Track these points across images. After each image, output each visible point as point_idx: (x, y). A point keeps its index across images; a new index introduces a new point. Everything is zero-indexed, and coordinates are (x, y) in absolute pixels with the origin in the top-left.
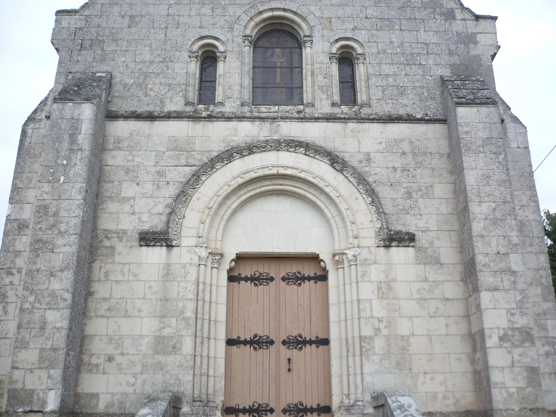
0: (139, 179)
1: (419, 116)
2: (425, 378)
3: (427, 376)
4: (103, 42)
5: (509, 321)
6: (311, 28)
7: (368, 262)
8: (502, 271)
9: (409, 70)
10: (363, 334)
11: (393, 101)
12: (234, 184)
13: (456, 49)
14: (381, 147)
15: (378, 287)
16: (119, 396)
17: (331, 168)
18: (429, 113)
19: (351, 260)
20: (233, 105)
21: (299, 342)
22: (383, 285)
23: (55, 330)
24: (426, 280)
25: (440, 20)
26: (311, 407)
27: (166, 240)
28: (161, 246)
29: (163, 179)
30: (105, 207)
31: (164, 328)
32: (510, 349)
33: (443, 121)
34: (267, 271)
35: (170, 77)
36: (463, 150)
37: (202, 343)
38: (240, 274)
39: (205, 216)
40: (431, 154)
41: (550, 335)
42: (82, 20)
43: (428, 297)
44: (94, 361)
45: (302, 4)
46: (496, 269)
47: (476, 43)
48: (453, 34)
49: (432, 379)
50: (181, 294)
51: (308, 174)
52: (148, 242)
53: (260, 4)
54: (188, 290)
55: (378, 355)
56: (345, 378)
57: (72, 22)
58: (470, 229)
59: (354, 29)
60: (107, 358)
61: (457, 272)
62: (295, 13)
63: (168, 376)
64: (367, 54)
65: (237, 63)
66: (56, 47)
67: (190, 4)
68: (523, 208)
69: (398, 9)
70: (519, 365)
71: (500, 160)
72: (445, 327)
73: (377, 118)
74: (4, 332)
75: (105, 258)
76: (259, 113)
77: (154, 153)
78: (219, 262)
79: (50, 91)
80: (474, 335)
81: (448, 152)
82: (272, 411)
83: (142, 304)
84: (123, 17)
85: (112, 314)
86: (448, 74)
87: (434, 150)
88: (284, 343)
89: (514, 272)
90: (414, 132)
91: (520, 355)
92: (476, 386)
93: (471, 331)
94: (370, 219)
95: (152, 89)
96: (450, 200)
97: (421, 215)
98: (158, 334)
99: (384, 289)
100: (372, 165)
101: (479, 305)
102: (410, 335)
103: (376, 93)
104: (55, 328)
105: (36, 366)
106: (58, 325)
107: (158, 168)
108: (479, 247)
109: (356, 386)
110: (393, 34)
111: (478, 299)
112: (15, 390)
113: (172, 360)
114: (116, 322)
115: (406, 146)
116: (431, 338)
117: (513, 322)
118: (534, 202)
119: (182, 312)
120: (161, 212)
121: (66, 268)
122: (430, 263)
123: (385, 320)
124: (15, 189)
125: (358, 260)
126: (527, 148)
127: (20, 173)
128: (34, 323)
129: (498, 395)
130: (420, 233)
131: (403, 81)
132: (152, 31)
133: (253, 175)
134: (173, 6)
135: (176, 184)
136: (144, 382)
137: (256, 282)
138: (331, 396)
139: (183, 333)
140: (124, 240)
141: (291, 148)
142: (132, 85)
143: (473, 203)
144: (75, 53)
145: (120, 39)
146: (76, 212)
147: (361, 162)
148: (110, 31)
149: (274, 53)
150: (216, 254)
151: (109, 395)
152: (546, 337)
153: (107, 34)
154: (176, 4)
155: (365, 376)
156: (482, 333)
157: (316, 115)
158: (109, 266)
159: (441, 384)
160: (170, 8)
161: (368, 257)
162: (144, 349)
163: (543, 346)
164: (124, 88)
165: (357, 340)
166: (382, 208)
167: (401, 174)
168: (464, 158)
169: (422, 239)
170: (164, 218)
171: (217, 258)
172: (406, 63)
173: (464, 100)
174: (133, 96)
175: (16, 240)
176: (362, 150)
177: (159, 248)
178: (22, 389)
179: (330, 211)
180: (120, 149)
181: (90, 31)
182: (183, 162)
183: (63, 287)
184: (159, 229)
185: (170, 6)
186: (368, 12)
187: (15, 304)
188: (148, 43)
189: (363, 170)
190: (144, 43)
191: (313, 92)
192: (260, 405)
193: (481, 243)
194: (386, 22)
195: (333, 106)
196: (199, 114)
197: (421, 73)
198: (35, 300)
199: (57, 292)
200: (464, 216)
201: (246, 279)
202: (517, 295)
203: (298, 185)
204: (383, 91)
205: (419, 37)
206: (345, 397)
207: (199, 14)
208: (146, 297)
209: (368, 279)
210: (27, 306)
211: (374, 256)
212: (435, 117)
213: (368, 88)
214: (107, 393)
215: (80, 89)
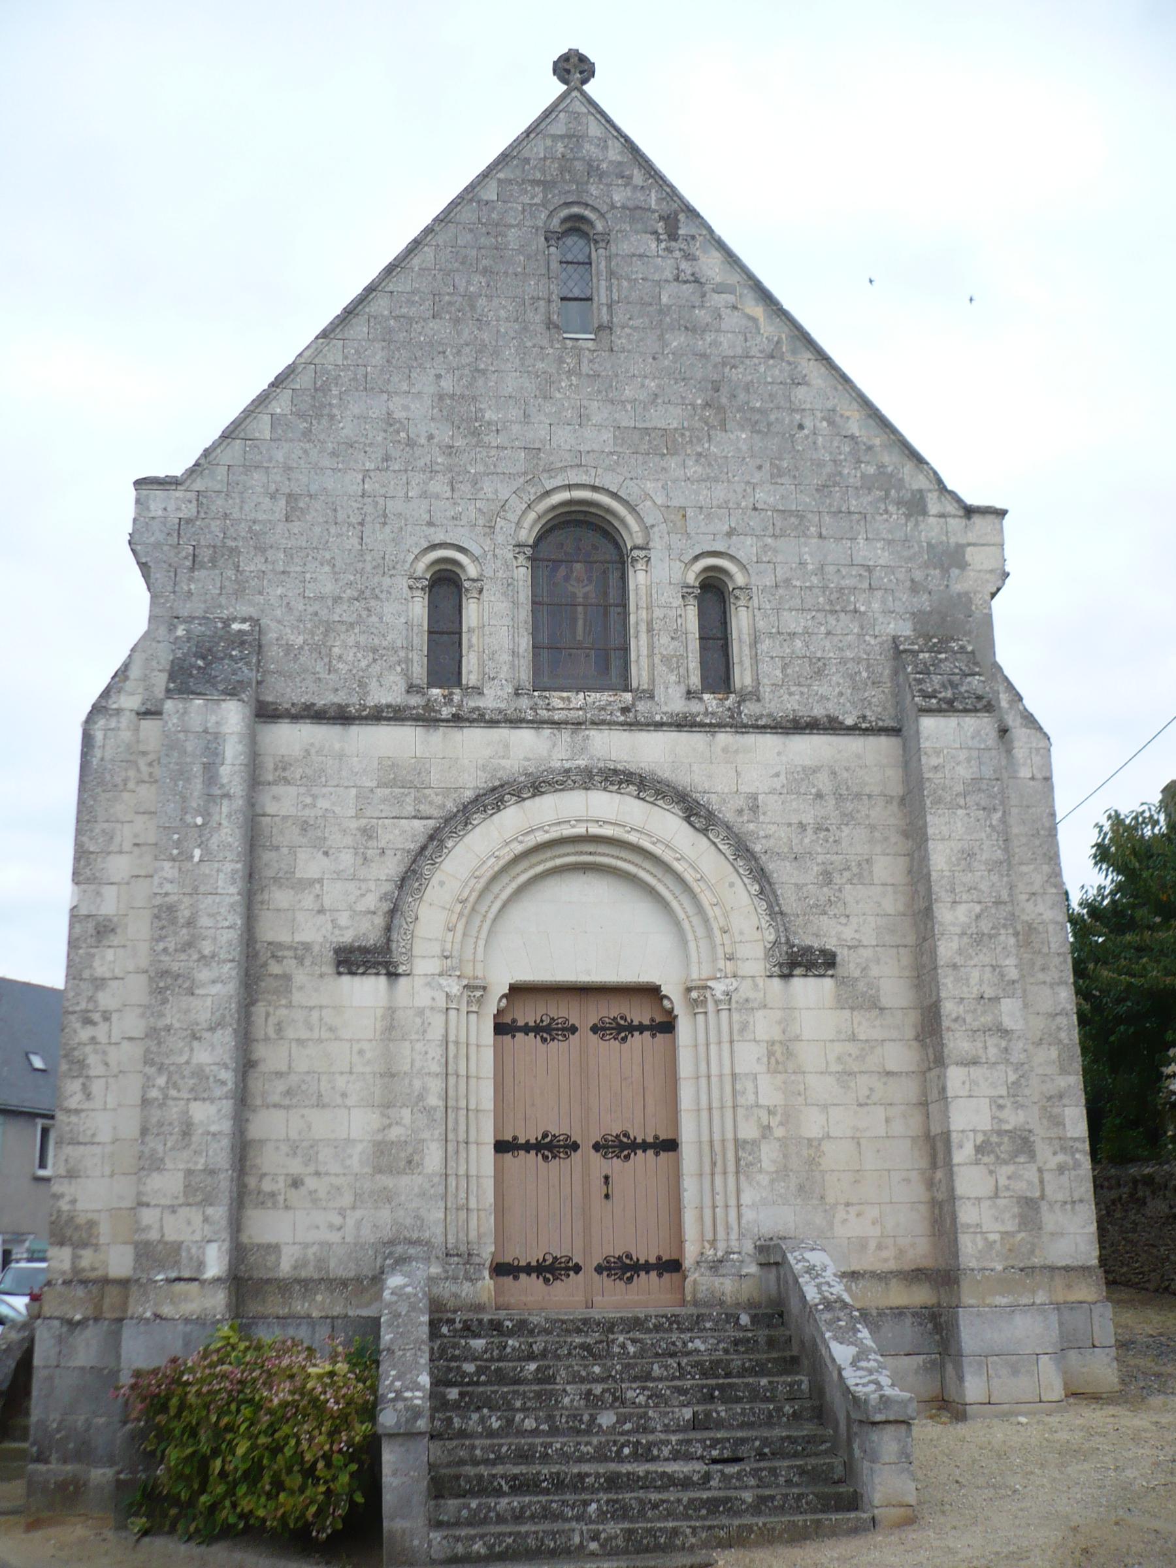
0: (328, 843)
1: (849, 722)
2: (848, 1212)
3: (850, 1209)
4: (234, 551)
5: (993, 1118)
6: (647, 529)
7: (751, 1005)
9: (834, 623)
10: (741, 1135)
11: (802, 689)
12: (507, 854)
13: (926, 579)
14: (778, 783)
15: (768, 1051)
16: (315, 1248)
17: (685, 824)
18: (868, 713)
19: (720, 1001)
20: (499, 693)
21: (623, 1146)
22: (778, 1048)
23: (209, 1137)
24: (853, 1038)
25: (896, 514)
26: (647, 1261)
27: (387, 964)
28: (377, 974)
30: (266, 897)
31: (390, 1126)
32: (992, 1168)
33: (895, 731)
34: (563, 1013)
35: (375, 631)
36: (928, 802)
37: (457, 1152)
38: (514, 1021)
39: (455, 916)
40: (870, 796)
41: (1069, 1135)
42: (190, 502)
43: (856, 1070)
44: (267, 1186)
45: (630, 476)
46: (975, 1025)
47: (963, 565)
48: (921, 547)
49: (858, 1215)
50: (418, 1065)
51: (643, 836)
52: (354, 969)
53: (546, 475)
54: (430, 1056)
55: (767, 1173)
56: (708, 1213)
57: (171, 507)
58: (933, 952)
59: (731, 533)
60: (290, 1181)
61: (909, 1023)
62: (614, 496)
63: (401, 1213)
64: (755, 589)
65: (505, 604)
66: (144, 560)
67: (406, 471)
69: (817, 490)
70: (1007, 1194)
71: (994, 823)
72: (883, 1122)
73: (773, 724)
74: (89, 1133)
75: (275, 997)
76: (549, 710)
77: (354, 791)
78: (480, 1001)
79: (132, 650)
80: (935, 1136)
81: (901, 793)
82: (577, 1269)
83: (348, 1082)
84: (273, 497)
85: (294, 1101)
86: (908, 633)
87: (876, 790)
88: (597, 1147)
89: (1007, 1031)
90: (839, 752)
91: (1009, 1178)
92: (933, 1227)
93: (929, 1131)
94: (757, 924)
95: (340, 657)
96: (900, 888)
97: (848, 916)
98: (379, 1137)
99: (778, 1055)
100: (762, 818)
101: (943, 1089)
102: (823, 1139)
103: (771, 672)
104: (208, 1133)
105: (181, 1200)
106: (213, 1128)
108: (949, 987)
109: (728, 1227)
110: (806, 544)
111: (942, 1077)
112: (147, 1243)
114: (303, 1116)
115: (823, 782)
116: (859, 1144)
117: (1001, 1121)
119: (421, 1097)
120: (372, 908)
121: (219, 1024)
122: (862, 1008)
123: (780, 1110)
124: (82, 855)
125: (733, 1001)
126: (1048, 779)
127: (88, 821)
129: (969, 1244)
130: (845, 951)
131: (824, 648)
132: (333, 530)
133: (542, 837)
134: (372, 474)
135: (399, 853)
136: (359, 1224)
137: (545, 1035)
138: (681, 1242)
139: (426, 1135)
140: (307, 962)
141: (612, 784)
142: (301, 648)
143: (941, 905)
144: (183, 573)
145: (271, 547)
146: (229, 917)
147: (740, 812)
148: (250, 527)
149: (572, 572)
150: (476, 988)
151: (297, 1247)
152: (1060, 1138)
153: (243, 534)
154: (378, 469)
155: (744, 1210)
156: (946, 1136)
157: (658, 718)
158: (283, 1012)
159: (873, 1224)
160: (367, 479)
161: (751, 995)
162: (355, 1163)
163: (1055, 1153)
164: (287, 653)
165: (730, 1147)
166: (778, 905)
167: (814, 837)
168: (929, 818)
169: (849, 963)
170: (379, 921)
171: (478, 994)
172: (828, 608)
173: (934, 701)
174: (306, 671)
175: (93, 956)
176: (744, 789)
177: (373, 979)
178: (159, 1242)
179: (681, 906)
180: (287, 781)
181: (208, 526)
182: (410, 810)
183: (218, 1060)
184: (372, 942)
185: (366, 474)
186: (757, 496)
187: (104, 1080)
188: (328, 557)
189: (744, 830)
190: (319, 557)
191: (652, 667)
192: (555, 1258)
193: (951, 978)
194: (793, 519)
195: (689, 699)
196: (435, 711)
197: (856, 631)
198: (167, 1083)
199: (207, 1069)
200: (926, 925)
201: (526, 1029)
202: (1010, 1073)
203: (623, 854)
204: (784, 668)
205: (854, 553)
206: (707, 1245)
207: (424, 495)
208: (354, 1070)
209: (751, 1037)
210: (154, 1093)
211: (761, 995)
212: (880, 724)
213: (755, 659)
214: (294, 1244)
215: (208, 664)
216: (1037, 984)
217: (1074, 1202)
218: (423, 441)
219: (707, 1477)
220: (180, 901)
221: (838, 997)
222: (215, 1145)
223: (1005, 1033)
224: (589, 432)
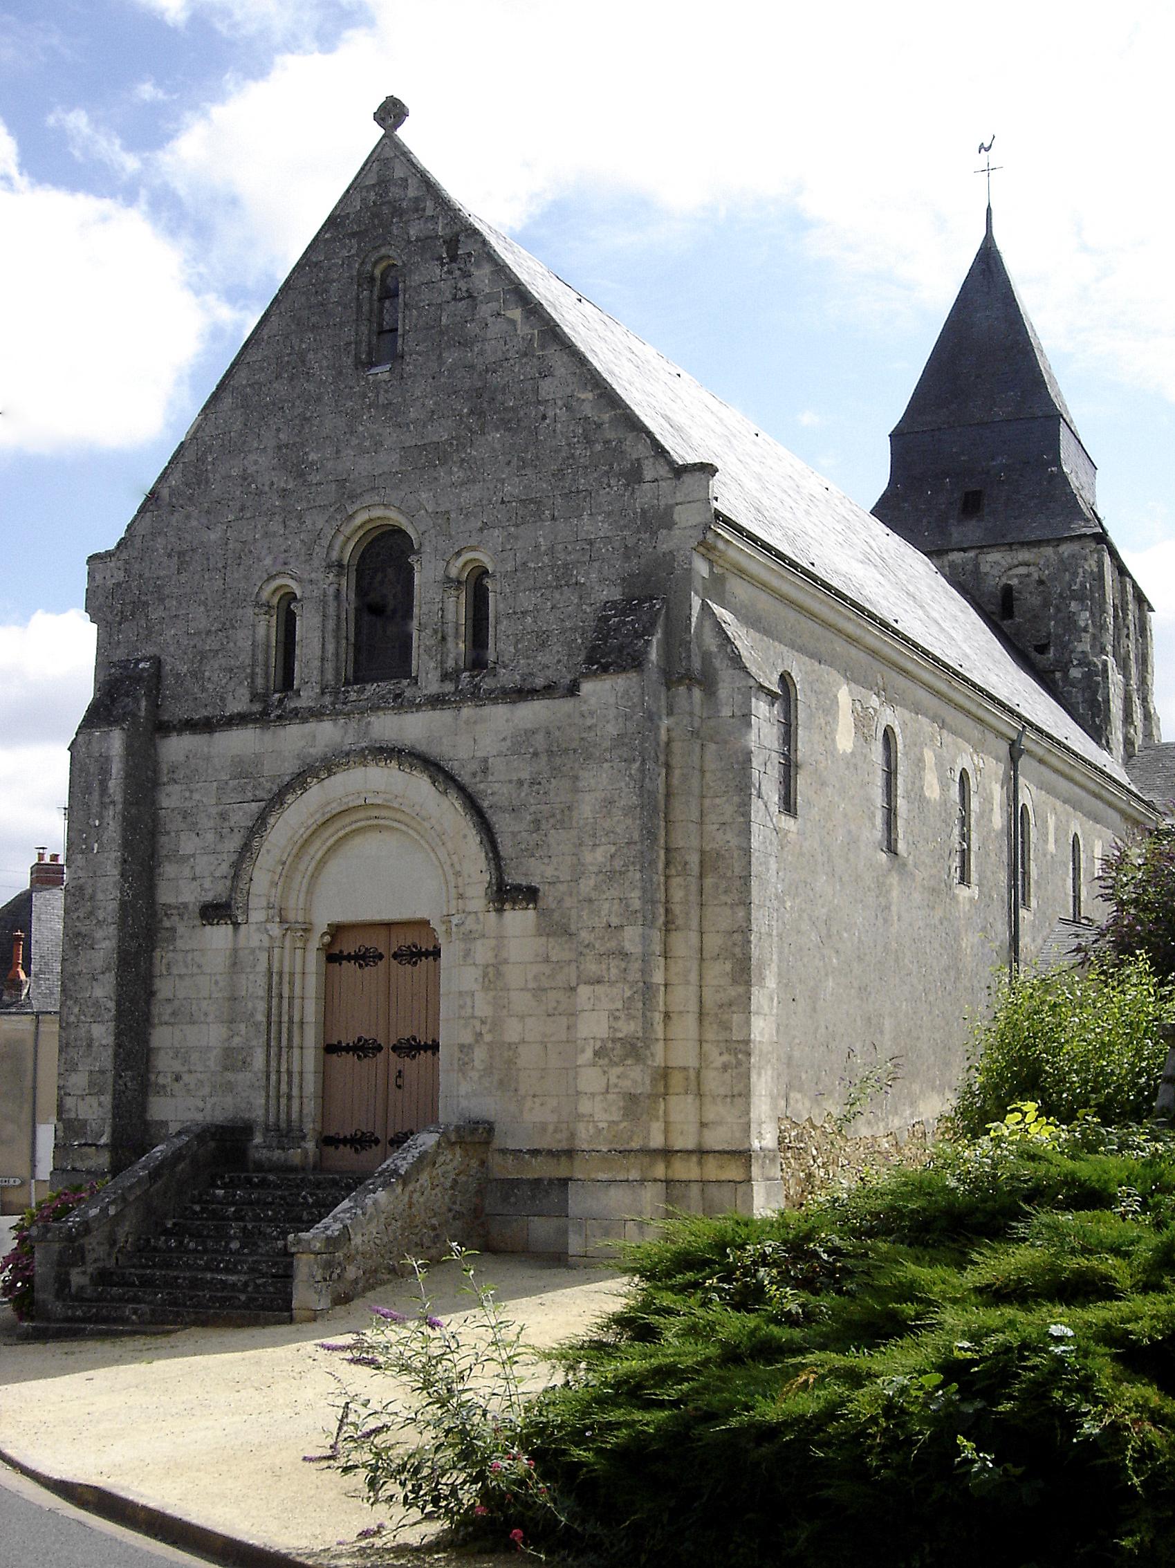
0: (199, 826)
3: (535, 1099)
4: (146, 604)
8: (610, 954)
24: (547, 960)
25: (617, 484)
26: (345, 1146)
29: (226, 824)
32: (606, 1069)
38: (341, 952)
40: (575, 751)
44: (161, 1081)
47: (669, 524)
50: (250, 990)
53: (349, 502)
55: (478, 1071)
68: (724, 827)
84: (169, 556)
88: (394, 1048)
91: (618, 1077)
99: (491, 975)
106: (104, 1042)
107: (221, 807)
113: (243, 1078)
115: (540, 741)
117: (615, 1030)
118: (743, 815)
119: (252, 1015)
128: (81, 1039)
129: (583, 1131)
139: (254, 1043)
140: (186, 917)
147: (474, 775)
158: (171, 955)
161: (474, 927)
162: (211, 1063)
169: (549, 898)
176: (479, 754)
193: (587, 911)
199: (101, 1000)
201: (349, 958)
209: (471, 962)
216: (721, 905)
217: (733, 1096)
218: (267, 488)
219: (246, 1284)
220: (86, 883)
221: (538, 925)
222: (105, 1054)
223: (624, 955)
224: (382, 456)
